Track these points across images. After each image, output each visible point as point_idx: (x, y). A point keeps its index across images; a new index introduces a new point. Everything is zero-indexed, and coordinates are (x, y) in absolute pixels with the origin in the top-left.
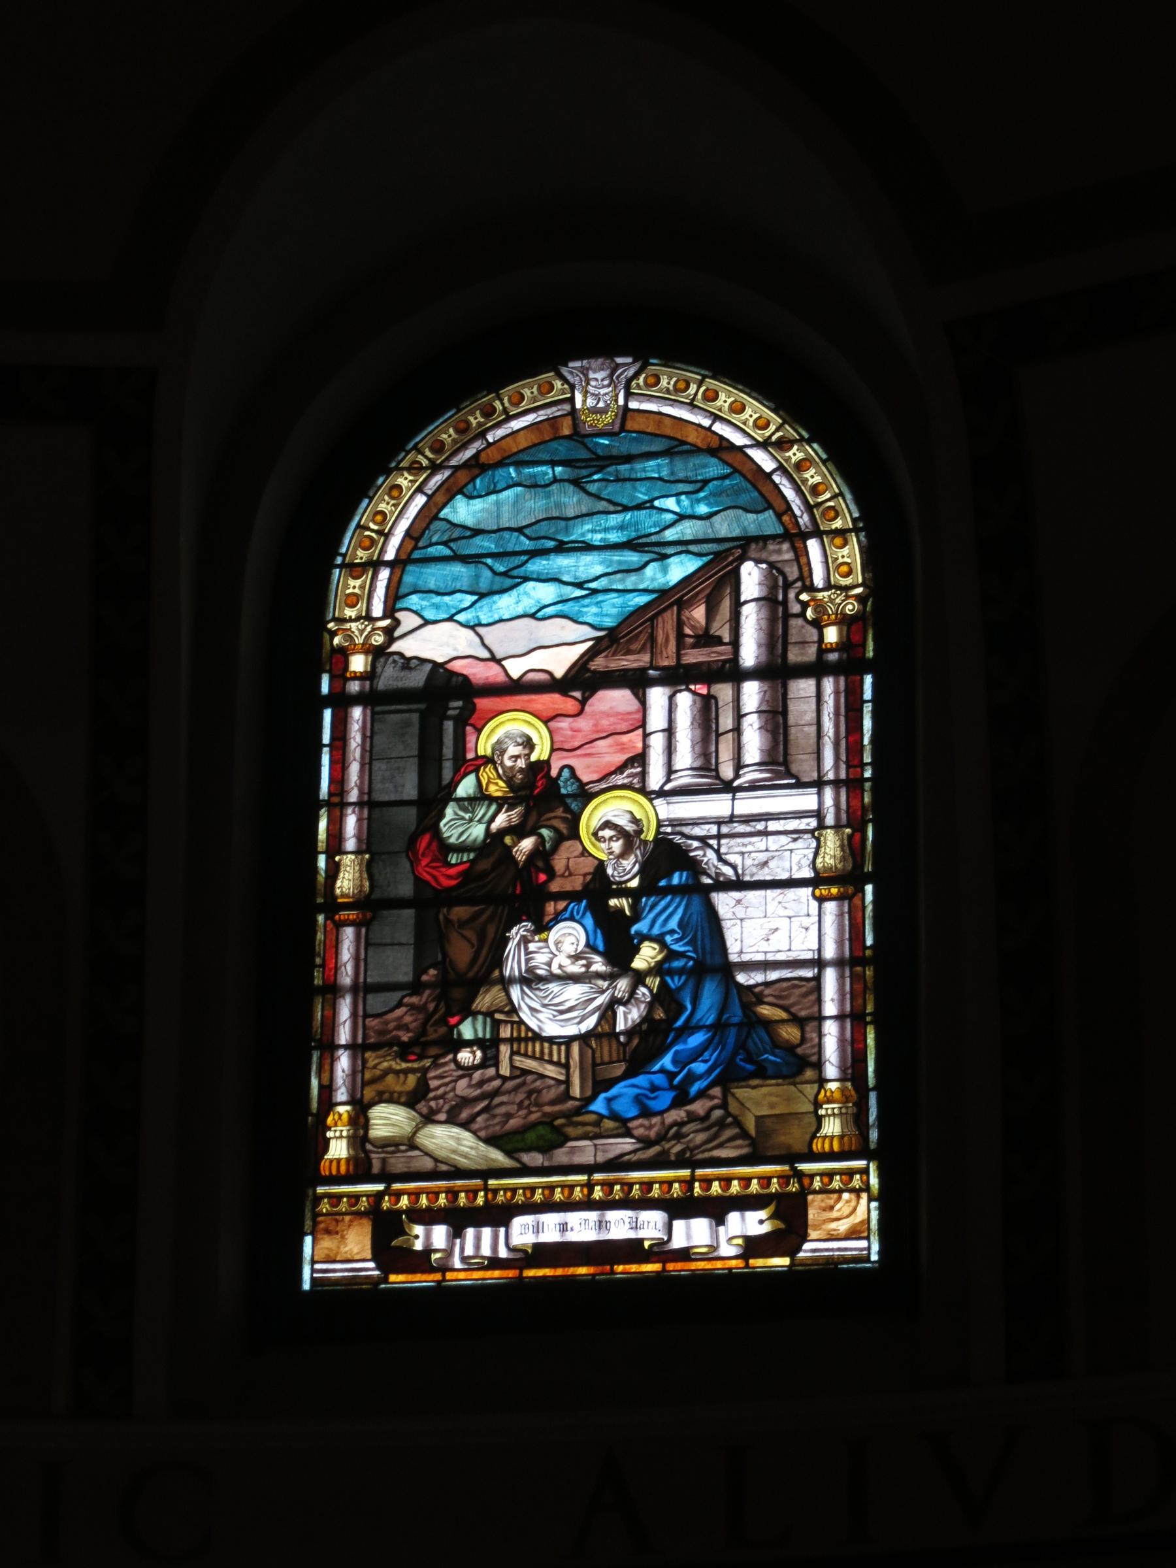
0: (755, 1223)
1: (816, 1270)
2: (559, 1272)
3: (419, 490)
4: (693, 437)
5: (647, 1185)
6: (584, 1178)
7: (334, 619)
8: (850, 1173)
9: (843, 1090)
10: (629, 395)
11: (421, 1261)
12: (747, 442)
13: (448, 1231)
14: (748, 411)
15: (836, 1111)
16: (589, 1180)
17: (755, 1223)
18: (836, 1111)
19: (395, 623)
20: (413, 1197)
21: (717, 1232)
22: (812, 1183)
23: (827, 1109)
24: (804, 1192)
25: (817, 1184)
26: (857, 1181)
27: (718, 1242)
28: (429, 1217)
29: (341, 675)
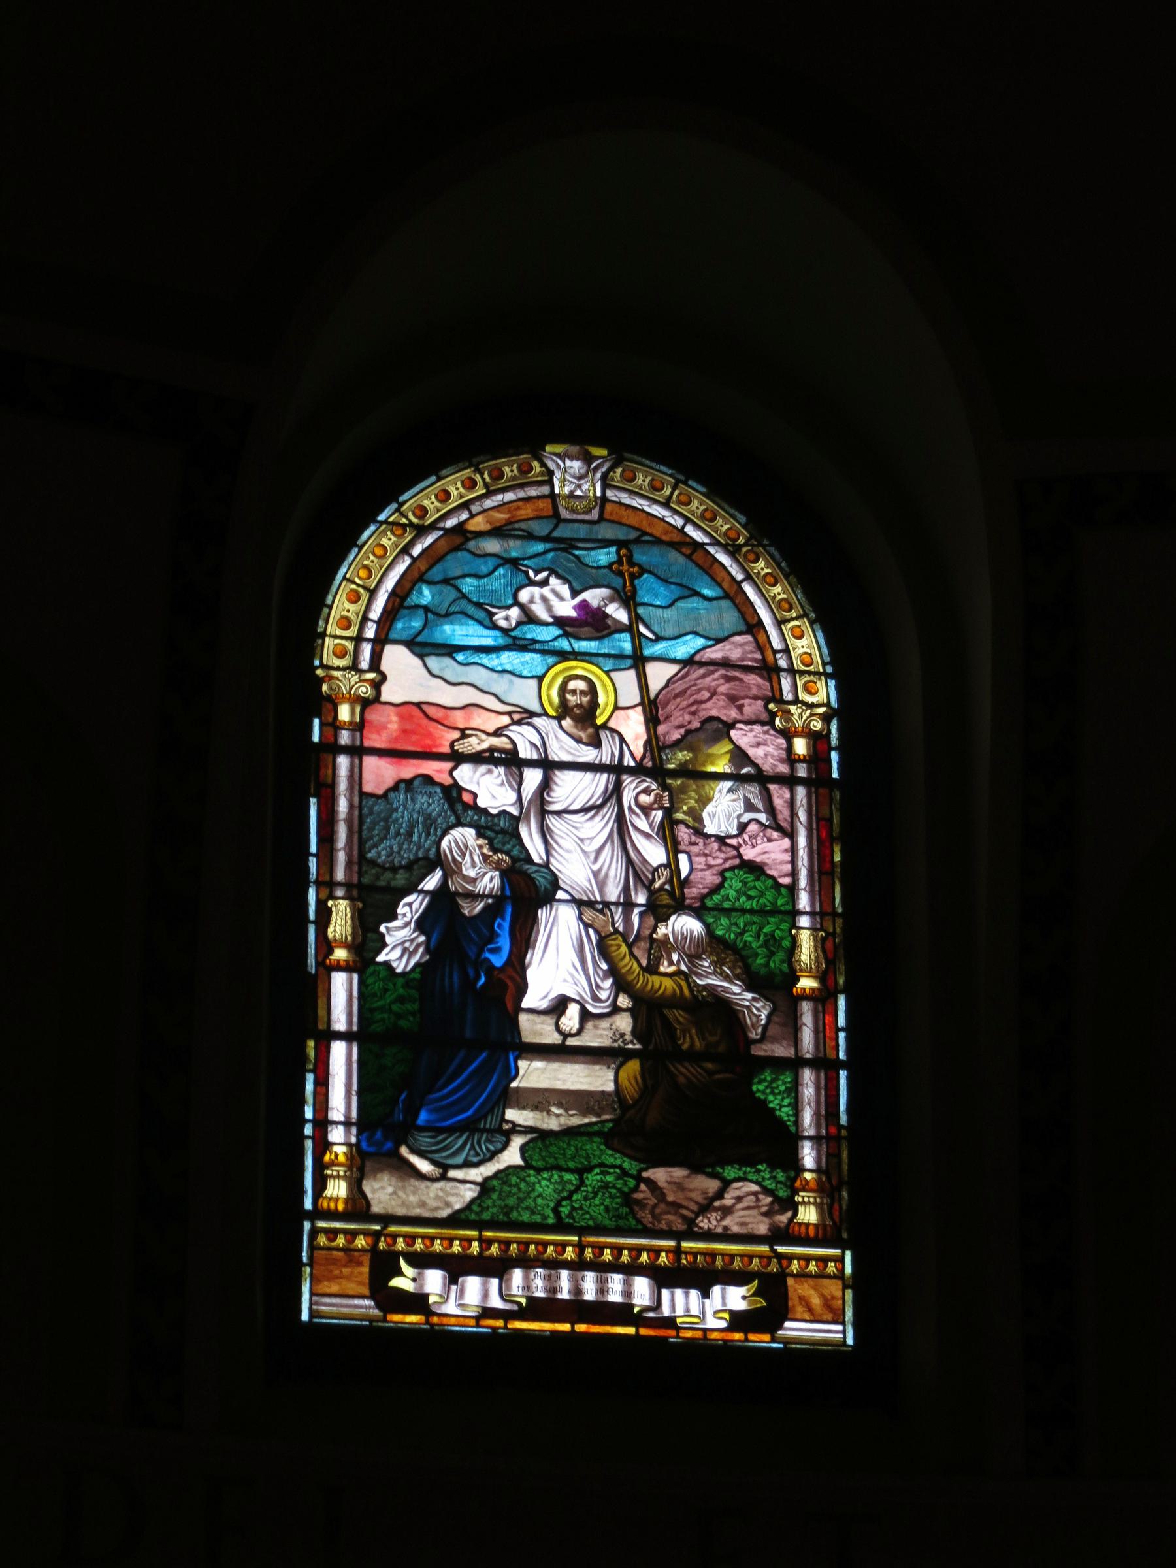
0: (736, 1298)
1: (828, 1351)
2: (547, 1326)
3: (406, 550)
4: (657, 531)
5: (637, 1251)
6: (672, 1243)
7: (322, 666)
8: (824, 1260)
9: (819, 1181)
10: (605, 486)
11: (418, 1302)
12: (706, 540)
13: (444, 1277)
14: (452, 489)
15: (812, 1200)
16: (580, 1241)
17: (736, 1298)
18: (342, 1173)
19: (379, 678)
20: (634, 1253)
21: (449, 1288)
22: (790, 1264)
23: (803, 1197)
24: (783, 1275)
25: (795, 1266)
26: (831, 1268)
27: (704, 1313)
28: (422, 1261)
29: (333, 726)
